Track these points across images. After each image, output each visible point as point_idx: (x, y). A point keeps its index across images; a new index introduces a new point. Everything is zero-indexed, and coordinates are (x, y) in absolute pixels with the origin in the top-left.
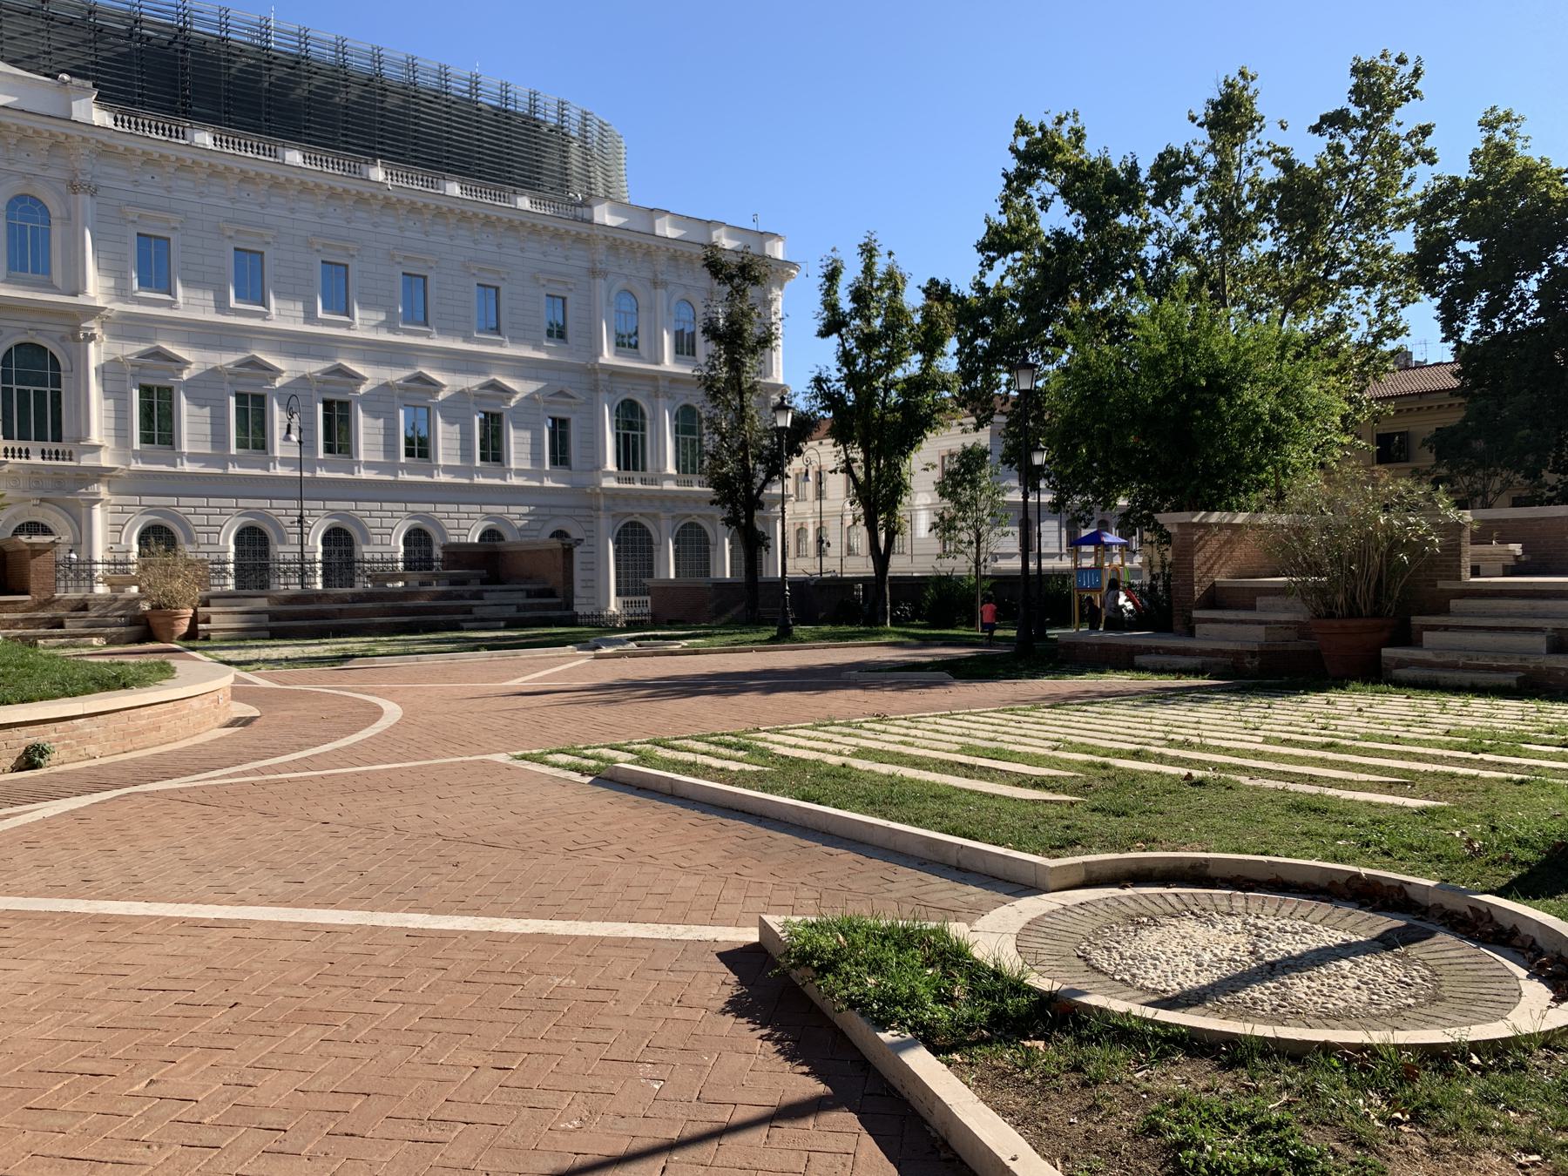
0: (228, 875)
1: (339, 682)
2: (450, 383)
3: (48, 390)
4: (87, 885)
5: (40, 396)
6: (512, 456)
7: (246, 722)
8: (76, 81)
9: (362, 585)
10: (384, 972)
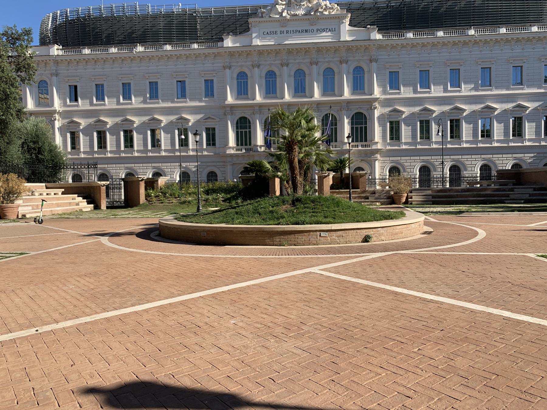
0: (432, 285)
1: (460, 221)
2: (499, 107)
3: (363, 126)
4: (388, 281)
5: (246, 132)
6: (527, 133)
7: (430, 233)
8: (372, 27)
9: (464, 186)
10: (496, 330)
